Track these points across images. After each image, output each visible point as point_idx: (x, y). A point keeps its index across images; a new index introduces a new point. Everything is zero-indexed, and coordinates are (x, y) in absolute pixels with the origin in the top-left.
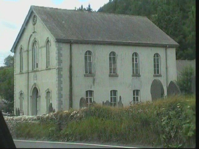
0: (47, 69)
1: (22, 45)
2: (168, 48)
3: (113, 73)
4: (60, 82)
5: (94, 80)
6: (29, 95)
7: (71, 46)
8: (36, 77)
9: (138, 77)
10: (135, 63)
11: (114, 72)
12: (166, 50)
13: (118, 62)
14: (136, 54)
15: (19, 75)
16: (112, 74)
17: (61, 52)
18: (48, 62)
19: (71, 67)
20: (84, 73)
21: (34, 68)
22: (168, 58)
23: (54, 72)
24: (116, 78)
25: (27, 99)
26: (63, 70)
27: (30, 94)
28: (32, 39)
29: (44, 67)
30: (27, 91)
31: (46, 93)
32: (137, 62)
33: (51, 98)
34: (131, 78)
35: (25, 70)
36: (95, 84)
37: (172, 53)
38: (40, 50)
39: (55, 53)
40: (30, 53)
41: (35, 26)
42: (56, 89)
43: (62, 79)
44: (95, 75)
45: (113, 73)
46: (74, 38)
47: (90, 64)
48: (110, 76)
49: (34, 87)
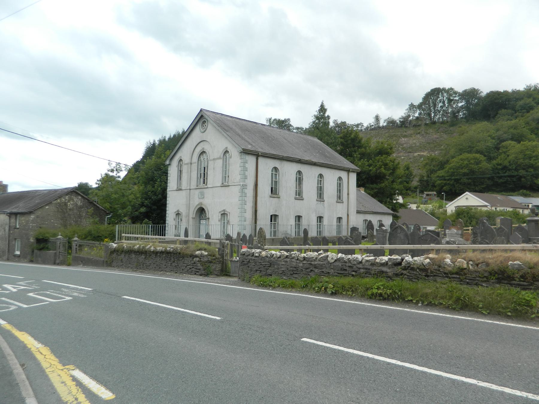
3: (299, 195)
8: (202, 196)
17: (247, 165)
18: (225, 177)
19: (256, 185)
23: (235, 190)
26: (248, 188)
27: (192, 213)
33: (181, 220)
34: (315, 202)
35: (184, 185)
37: (353, 177)
45: (299, 195)
49: (199, 207)
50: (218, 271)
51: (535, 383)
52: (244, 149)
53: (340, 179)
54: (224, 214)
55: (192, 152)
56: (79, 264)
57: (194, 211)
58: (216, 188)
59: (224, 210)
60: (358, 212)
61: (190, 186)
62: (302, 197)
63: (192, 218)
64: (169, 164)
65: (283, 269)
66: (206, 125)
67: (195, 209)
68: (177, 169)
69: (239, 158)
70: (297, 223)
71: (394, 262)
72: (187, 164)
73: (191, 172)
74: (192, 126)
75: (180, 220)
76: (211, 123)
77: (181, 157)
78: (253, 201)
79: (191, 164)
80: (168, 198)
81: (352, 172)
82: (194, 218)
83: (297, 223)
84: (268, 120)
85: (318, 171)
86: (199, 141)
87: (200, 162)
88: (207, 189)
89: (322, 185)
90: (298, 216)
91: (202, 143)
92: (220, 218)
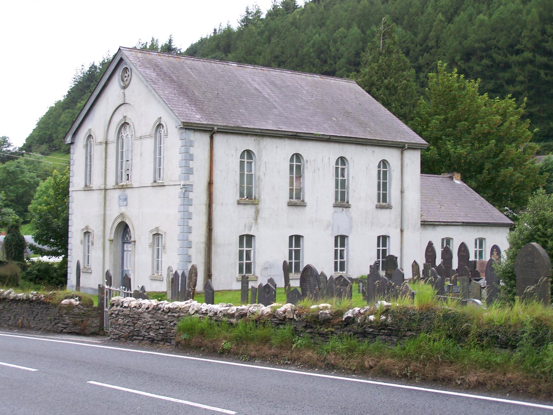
0: (154, 184)
1: (93, 130)
2: (406, 149)
4: (187, 216)
5: (257, 212)
6: (108, 237)
7: (212, 138)
9: (345, 209)
10: (246, 173)
11: (298, 197)
12: (402, 153)
13: (308, 175)
14: (342, 160)
15: (83, 192)
16: (294, 200)
17: (192, 150)
18: (158, 171)
19: (210, 184)
20: (238, 198)
21: (119, 180)
22: (405, 170)
23: (175, 192)
24: (301, 209)
25: (101, 245)
26: (194, 190)
27: (110, 234)
28: (118, 119)
29: (149, 181)
30: (102, 227)
31: (83, 234)
32: (344, 177)
33: (92, 244)
34: (332, 210)
35: (97, 181)
36: (259, 221)
38: (137, 143)
39: (178, 151)
40: (112, 148)
41: (127, 91)
42: (178, 229)
43: (191, 209)
44: (259, 202)
46: (220, 123)
47: (250, 177)
48: (290, 205)
49: (119, 220)
50: (95, 327)
52: (184, 123)
53: (384, 163)
54: (158, 234)
55: (108, 122)
59: (157, 228)
60: (425, 224)
62: (303, 201)
64: (72, 143)
65: (150, 323)
66: (129, 75)
67: (114, 223)
68: (84, 151)
69: (178, 138)
70: (294, 248)
71: (241, 312)
72: (101, 143)
75: (90, 244)
76: (135, 73)
77: (90, 130)
78: (206, 212)
81: (409, 148)
82: (112, 241)
83: (294, 248)
85: (336, 151)
86: (117, 105)
87: (120, 140)
88: (132, 189)
89: (346, 178)
90: (295, 236)
91: (122, 108)
92: (151, 241)
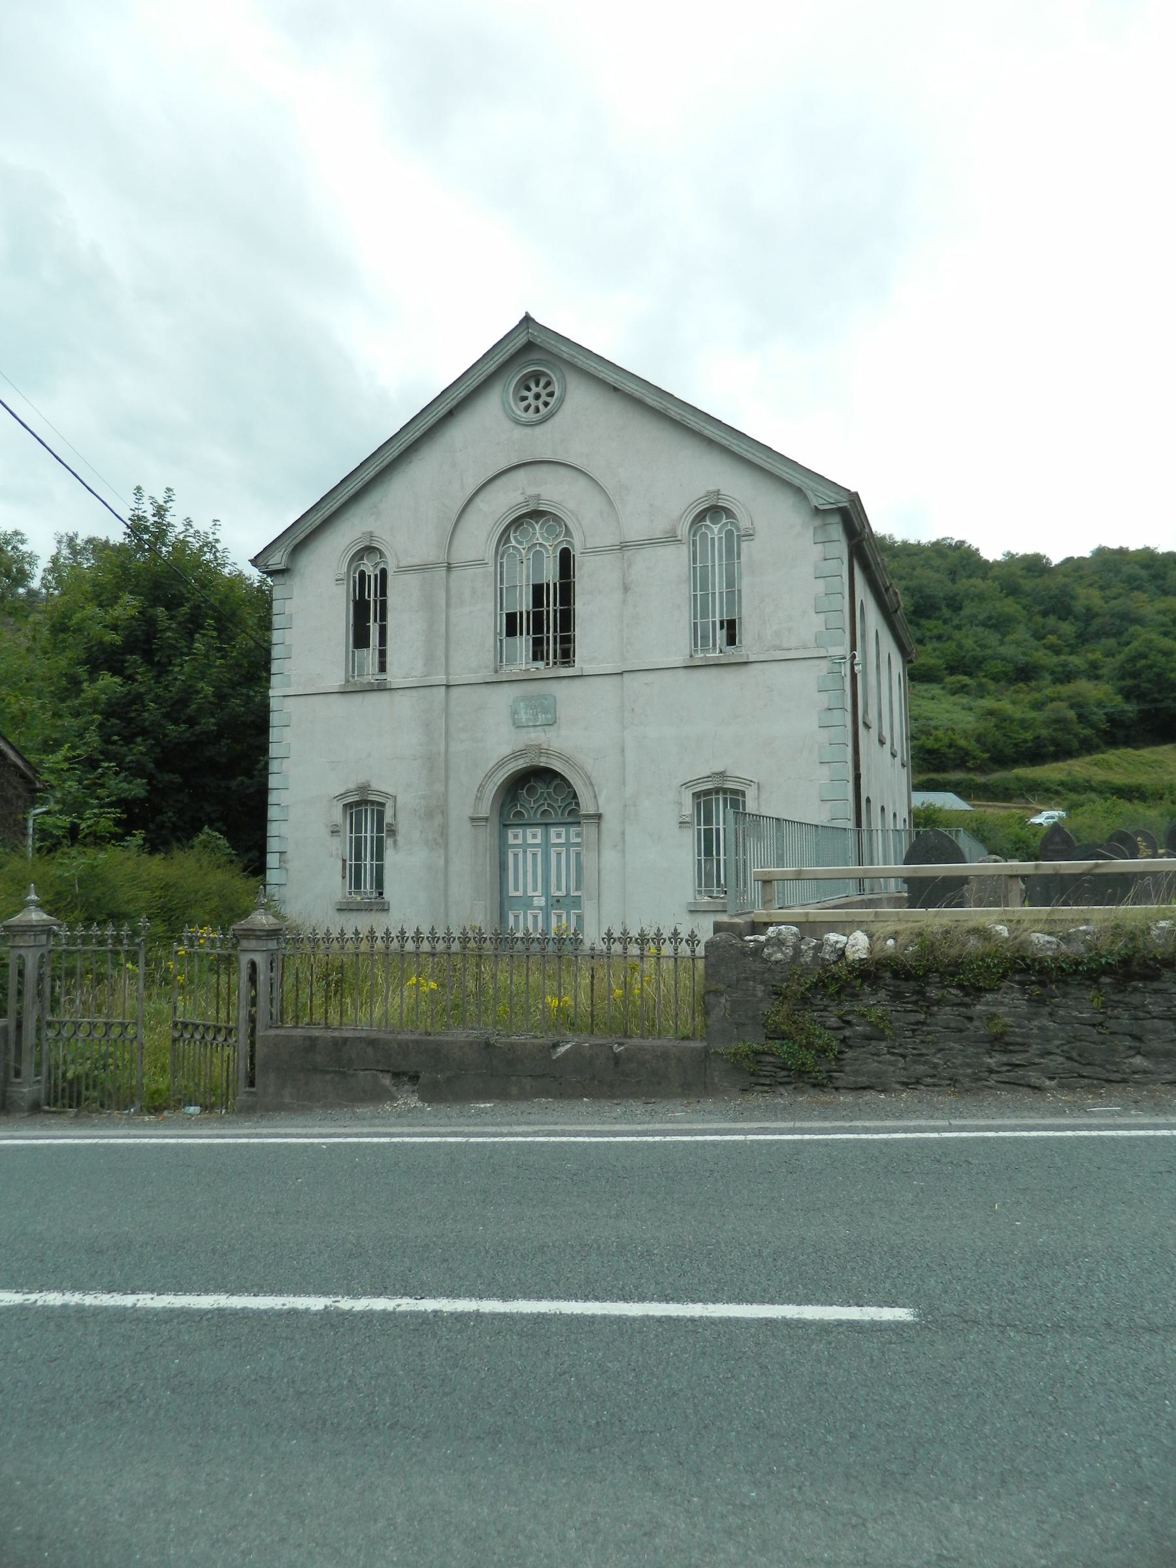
51: (1171, 1326)
56: (377, 1096)
57: (481, 787)
58: (650, 677)
61: (447, 673)
63: (473, 819)
73: (448, 605)
74: (461, 392)
79: (449, 567)
80: (274, 734)
84: (65, 540)
